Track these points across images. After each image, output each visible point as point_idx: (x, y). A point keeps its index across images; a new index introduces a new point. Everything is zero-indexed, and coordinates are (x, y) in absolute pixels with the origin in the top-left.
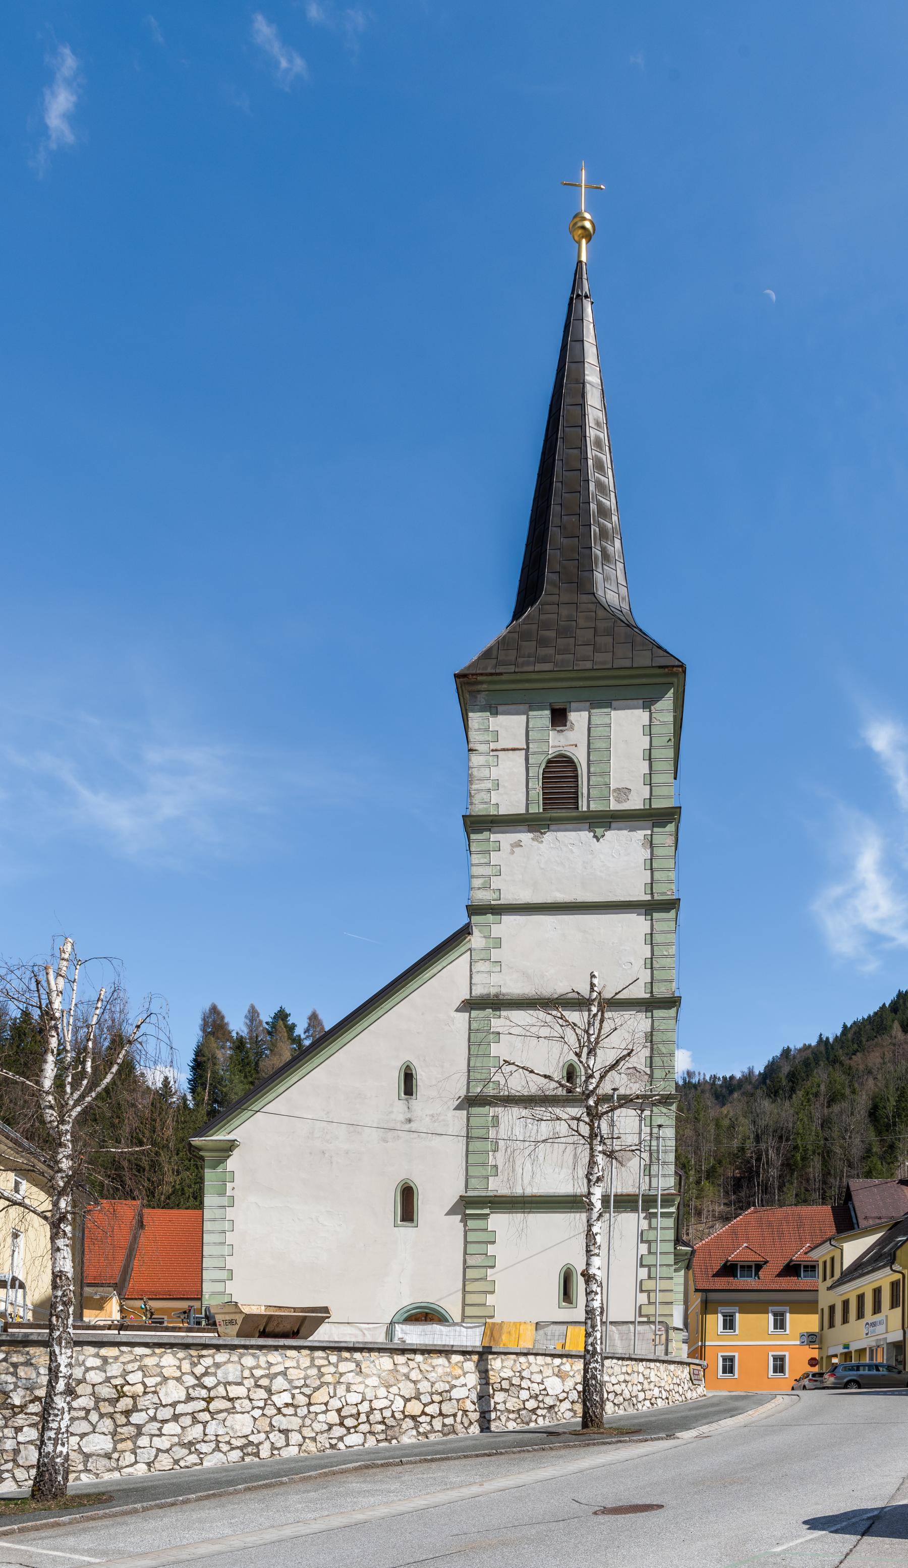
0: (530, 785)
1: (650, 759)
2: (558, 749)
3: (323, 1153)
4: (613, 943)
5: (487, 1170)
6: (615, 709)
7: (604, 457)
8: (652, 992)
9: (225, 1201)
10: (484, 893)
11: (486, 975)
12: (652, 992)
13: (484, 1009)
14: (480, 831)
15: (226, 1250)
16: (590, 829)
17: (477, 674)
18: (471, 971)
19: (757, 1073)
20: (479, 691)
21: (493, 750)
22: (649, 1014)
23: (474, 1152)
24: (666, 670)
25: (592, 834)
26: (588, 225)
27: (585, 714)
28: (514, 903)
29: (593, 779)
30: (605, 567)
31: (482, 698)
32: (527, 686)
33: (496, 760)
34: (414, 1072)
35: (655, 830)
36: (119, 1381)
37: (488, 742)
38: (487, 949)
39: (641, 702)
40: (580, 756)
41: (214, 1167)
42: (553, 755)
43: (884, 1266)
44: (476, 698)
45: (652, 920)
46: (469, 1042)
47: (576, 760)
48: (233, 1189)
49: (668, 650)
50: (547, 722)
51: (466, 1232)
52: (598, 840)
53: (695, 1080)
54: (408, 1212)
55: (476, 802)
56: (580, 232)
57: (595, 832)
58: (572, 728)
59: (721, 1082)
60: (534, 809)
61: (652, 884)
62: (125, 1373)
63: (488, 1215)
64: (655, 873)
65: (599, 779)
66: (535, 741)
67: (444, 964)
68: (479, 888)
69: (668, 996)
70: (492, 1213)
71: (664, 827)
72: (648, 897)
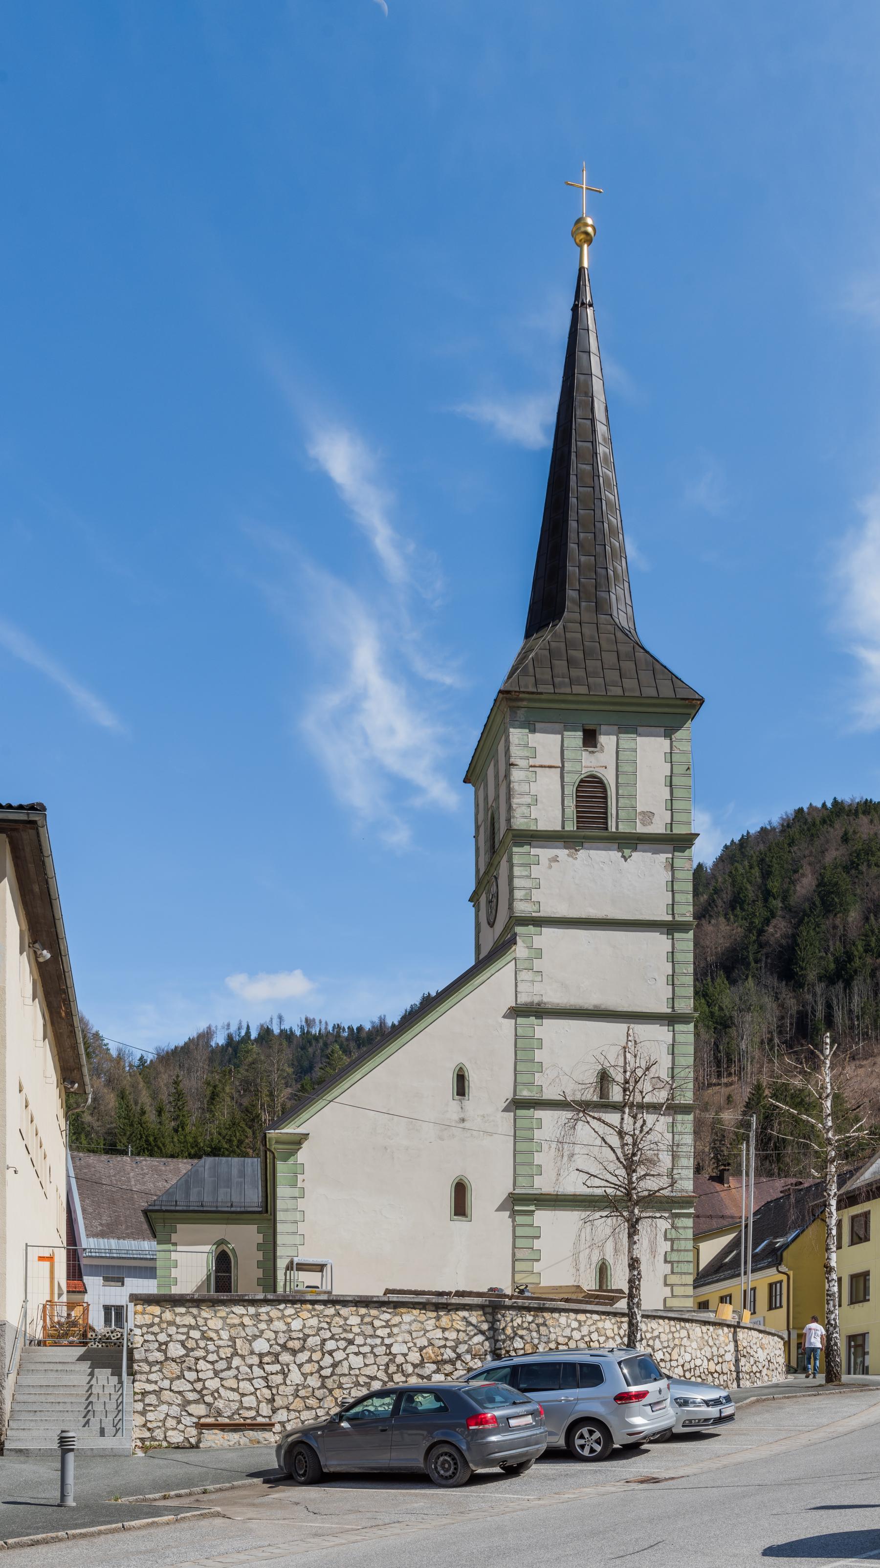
0: (566, 802)
1: (671, 786)
2: (592, 769)
3: (386, 1148)
4: (639, 959)
5: (532, 1169)
6: (640, 735)
7: (610, 474)
8: (673, 1008)
9: (296, 1192)
10: (526, 904)
11: (529, 984)
12: (673, 1008)
13: (528, 1016)
14: (521, 845)
15: (298, 1240)
16: (620, 849)
17: (519, 692)
18: (516, 979)
19: (389, 1024)
20: (519, 707)
21: (531, 766)
22: (671, 1028)
23: (521, 1152)
24: (687, 702)
25: (620, 854)
26: (590, 230)
27: (614, 738)
28: (552, 916)
29: (621, 801)
30: (617, 587)
31: (521, 714)
32: (563, 706)
33: (534, 775)
34: (466, 1074)
35: (676, 854)
36: (587, 1339)
37: (528, 758)
38: (530, 959)
39: (662, 729)
40: (609, 777)
41: (285, 1159)
42: (586, 775)
43: (768, 1267)
44: (516, 713)
45: (673, 939)
46: (516, 1047)
47: (606, 782)
48: (304, 1181)
49: (682, 679)
50: (580, 742)
51: (514, 1227)
52: (626, 860)
53: (315, 1031)
54: (460, 1207)
55: (518, 816)
56: (582, 236)
57: (623, 853)
58: (602, 751)
59: (346, 1034)
60: (571, 827)
61: (673, 905)
62: (590, 1333)
63: (534, 1211)
64: (676, 895)
65: (627, 801)
66: (570, 760)
67: (493, 971)
68: (521, 900)
69: (688, 1012)
70: (537, 1209)
71: (683, 852)
72: (670, 918)
